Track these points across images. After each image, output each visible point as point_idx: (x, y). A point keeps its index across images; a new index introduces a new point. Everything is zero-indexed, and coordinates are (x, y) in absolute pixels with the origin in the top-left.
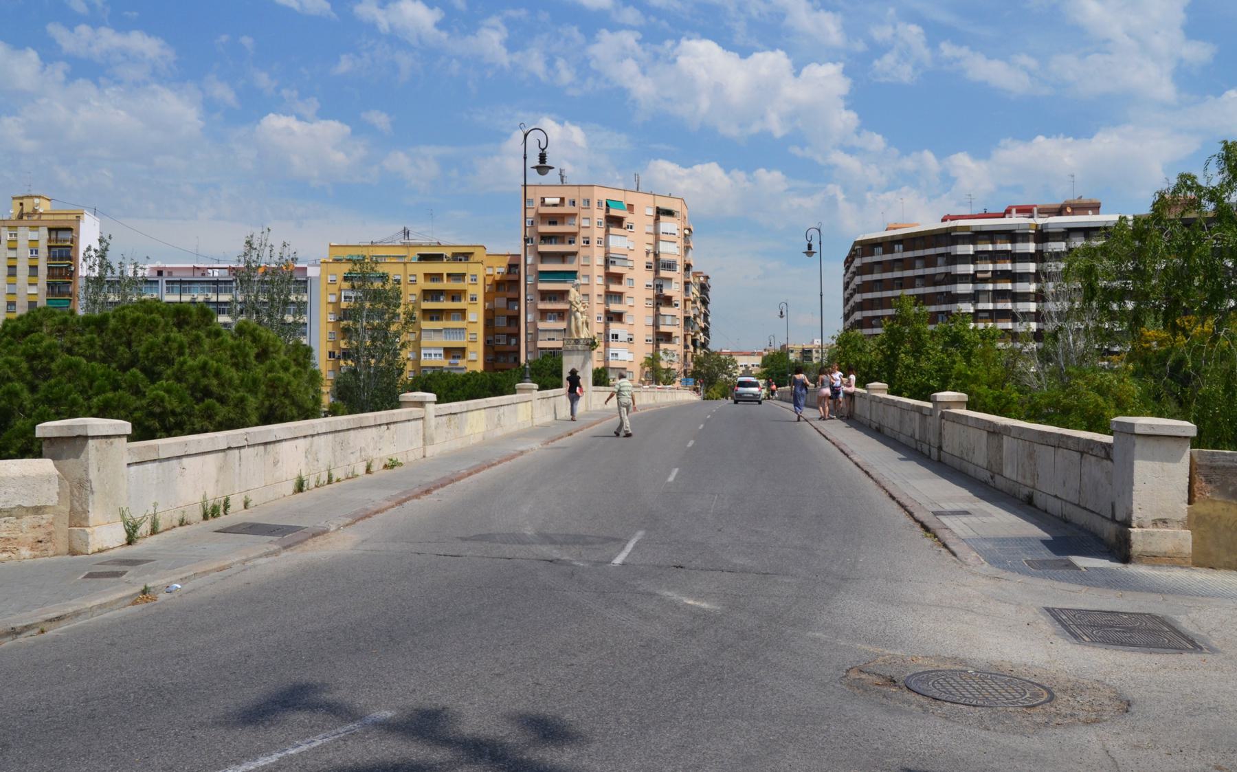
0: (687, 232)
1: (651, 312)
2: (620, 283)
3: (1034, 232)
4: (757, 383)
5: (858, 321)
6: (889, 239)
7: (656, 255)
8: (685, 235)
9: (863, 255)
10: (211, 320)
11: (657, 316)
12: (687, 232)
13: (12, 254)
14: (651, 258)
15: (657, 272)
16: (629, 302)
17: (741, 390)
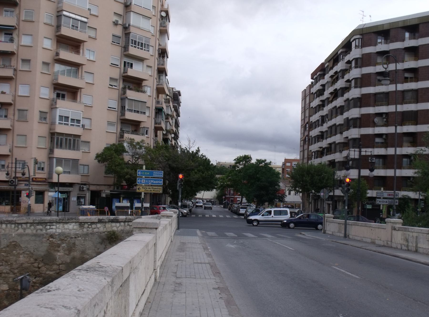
0: (164, 14)
1: (115, 94)
2: (78, 52)
3: (355, 166)
4: (43, 202)
5: (354, 140)
6: (401, 25)
7: (126, 28)
8: (162, 17)
9: (363, 45)
10: (214, 177)
11: (123, 99)
12: (164, 14)
13: (63, 124)
14: (118, 31)
15: (126, 48)
16: (25, 41)
17: (197, 204)
